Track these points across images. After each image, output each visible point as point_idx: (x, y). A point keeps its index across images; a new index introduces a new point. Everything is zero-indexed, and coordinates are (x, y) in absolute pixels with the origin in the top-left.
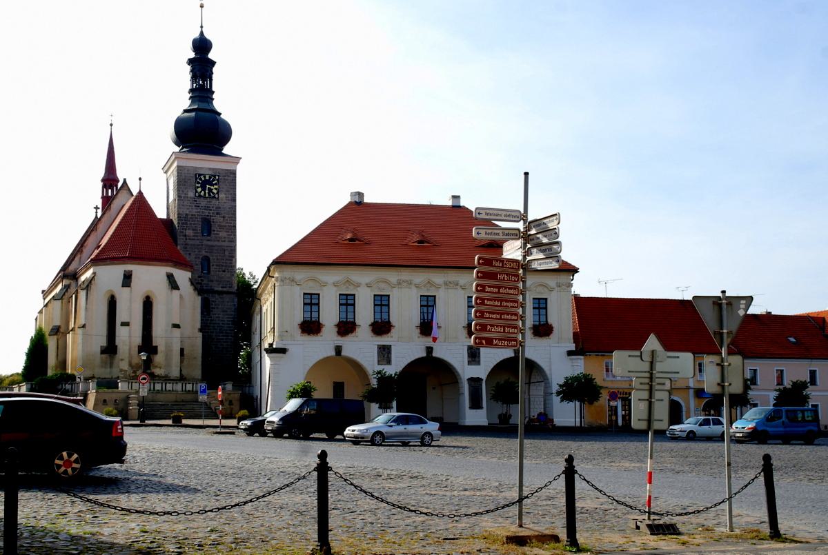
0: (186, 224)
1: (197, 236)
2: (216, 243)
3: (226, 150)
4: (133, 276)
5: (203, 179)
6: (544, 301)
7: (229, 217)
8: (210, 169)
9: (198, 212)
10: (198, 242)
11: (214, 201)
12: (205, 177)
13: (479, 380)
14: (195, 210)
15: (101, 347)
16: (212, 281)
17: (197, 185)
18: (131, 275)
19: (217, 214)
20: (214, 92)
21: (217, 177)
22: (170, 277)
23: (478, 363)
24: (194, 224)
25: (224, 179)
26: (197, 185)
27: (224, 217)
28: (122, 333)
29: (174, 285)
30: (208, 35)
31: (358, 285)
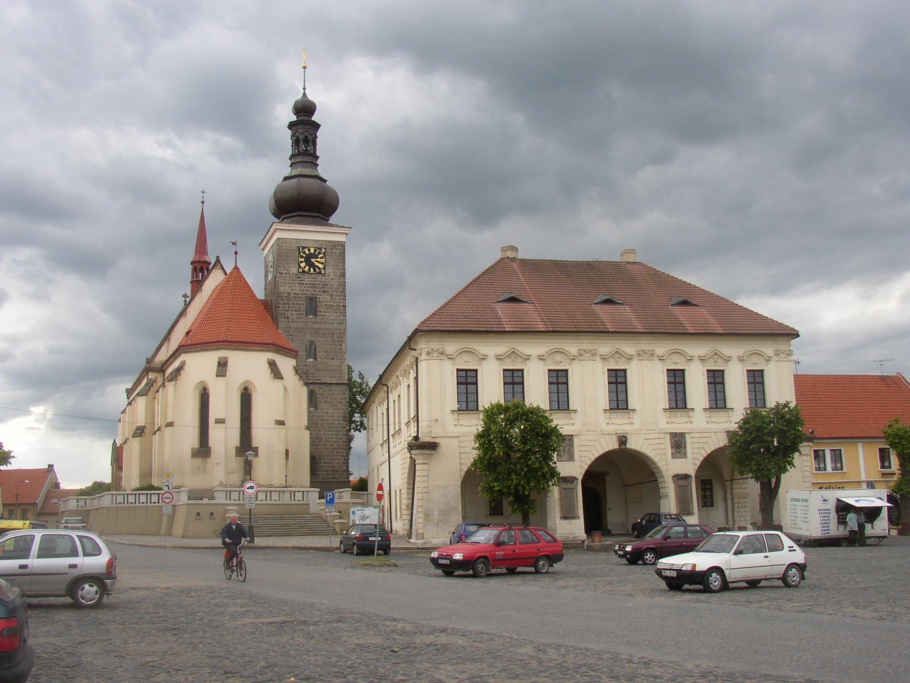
0: (288, 304)
1: (301, 318)
2: (323, 326)
3: (332, 220)
4: (229, 364)
5: (308, 252)
6: (681, 372)
7: (338, 296)
8: (315, 241)
9: (301, 290)
10: (301, 325)
11: (320, 277)
12: (309, 250)
13: (686, 477)
14: (298, 288)
15: (305, 426)
16: (319, 370)
17: (301, 260)
18: (227, 362)
19: (324, 292)
20: (318, 157)
21: (323, 250)
22: (272, 365)
23: (685, 456)
24: (297, 304)
25: (332, 252)
26: (301, 260)
27: (331, 295)
28: (216, 434)
29: (277, 374)
30: (311, 97)
31: (527, 358)
